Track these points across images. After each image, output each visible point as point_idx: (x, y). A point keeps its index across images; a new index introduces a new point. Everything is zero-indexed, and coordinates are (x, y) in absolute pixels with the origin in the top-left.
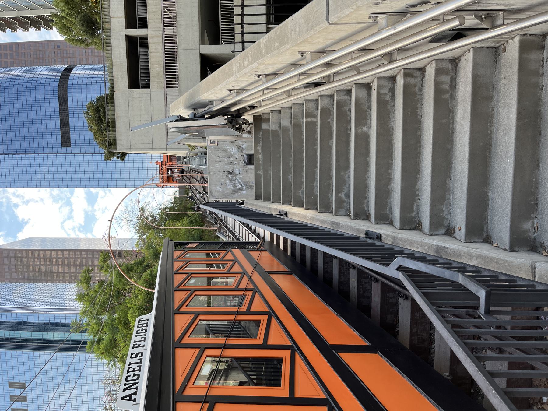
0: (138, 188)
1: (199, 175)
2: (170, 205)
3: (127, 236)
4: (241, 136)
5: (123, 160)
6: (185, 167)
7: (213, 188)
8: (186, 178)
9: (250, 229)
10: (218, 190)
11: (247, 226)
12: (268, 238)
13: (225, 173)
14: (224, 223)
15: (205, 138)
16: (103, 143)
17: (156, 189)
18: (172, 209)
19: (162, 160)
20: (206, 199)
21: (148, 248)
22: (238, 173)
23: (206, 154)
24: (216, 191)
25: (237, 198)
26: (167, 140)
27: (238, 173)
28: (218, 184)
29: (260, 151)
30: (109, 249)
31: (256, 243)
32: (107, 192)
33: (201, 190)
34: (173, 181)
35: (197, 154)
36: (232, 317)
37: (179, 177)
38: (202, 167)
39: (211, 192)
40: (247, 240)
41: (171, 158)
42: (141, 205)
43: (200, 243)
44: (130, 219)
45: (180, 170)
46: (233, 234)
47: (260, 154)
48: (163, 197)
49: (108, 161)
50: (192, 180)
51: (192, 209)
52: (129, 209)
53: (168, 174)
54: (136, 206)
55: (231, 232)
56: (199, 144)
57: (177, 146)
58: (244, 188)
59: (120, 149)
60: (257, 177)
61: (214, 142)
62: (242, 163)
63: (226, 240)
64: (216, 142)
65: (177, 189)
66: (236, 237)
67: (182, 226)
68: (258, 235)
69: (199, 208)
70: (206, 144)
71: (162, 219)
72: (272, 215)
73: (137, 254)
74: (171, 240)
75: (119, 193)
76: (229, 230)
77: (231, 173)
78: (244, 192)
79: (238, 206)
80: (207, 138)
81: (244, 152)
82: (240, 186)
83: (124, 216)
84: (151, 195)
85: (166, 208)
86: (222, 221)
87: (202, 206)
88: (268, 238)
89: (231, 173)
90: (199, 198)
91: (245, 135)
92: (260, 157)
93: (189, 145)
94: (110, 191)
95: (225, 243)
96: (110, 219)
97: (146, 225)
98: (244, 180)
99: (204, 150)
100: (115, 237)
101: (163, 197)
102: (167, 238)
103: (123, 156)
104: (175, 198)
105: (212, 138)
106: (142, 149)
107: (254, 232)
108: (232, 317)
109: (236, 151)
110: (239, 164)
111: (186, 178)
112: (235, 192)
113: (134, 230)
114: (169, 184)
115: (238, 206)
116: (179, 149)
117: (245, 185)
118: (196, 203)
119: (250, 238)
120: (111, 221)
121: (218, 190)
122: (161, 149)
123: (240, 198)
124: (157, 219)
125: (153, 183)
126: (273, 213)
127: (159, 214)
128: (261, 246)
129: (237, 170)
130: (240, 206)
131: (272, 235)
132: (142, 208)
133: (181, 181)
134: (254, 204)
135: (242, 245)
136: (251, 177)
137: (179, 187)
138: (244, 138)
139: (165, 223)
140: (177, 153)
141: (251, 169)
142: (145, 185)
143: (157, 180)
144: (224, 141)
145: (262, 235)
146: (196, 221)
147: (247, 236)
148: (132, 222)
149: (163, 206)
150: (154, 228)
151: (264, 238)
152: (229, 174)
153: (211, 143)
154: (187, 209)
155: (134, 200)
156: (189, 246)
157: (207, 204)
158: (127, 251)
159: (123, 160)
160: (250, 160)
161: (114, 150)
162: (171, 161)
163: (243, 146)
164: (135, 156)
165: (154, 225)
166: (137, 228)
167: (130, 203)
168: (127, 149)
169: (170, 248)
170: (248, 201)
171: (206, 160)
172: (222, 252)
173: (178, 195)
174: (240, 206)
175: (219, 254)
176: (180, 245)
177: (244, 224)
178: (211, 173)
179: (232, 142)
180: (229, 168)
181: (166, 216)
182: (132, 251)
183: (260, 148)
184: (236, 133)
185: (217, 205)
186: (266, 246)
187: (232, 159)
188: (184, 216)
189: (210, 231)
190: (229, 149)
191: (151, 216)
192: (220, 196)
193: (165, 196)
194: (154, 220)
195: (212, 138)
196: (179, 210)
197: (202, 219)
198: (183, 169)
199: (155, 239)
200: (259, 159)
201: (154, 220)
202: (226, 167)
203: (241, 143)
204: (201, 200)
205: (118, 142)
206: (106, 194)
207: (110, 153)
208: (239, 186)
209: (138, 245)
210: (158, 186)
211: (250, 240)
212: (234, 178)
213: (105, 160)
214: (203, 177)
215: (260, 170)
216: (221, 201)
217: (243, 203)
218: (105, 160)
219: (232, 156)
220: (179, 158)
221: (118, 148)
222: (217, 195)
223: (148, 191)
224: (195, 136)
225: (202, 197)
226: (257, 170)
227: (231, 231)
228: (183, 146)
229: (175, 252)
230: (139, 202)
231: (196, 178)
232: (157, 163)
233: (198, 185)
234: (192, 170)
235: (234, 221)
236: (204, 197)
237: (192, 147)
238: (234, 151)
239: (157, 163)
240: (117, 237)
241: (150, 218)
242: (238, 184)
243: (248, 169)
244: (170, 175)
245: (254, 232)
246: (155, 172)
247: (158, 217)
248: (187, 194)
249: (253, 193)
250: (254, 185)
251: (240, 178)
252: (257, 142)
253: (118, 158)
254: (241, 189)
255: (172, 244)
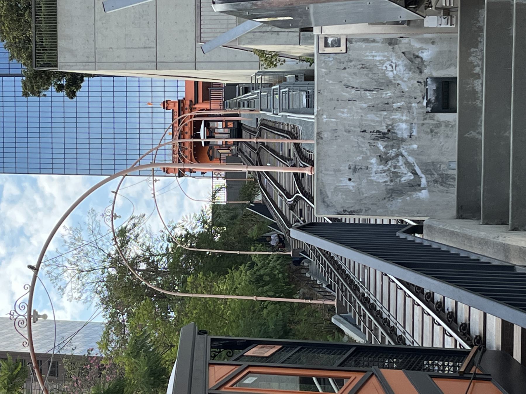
0: (112, 177)
1: (285, 141)
2: (199, 229)
3: (77, 313)
4: (419, 25)
5: (72, 95)
6: (246, 117)
7: (329, 180)
8: (247, 150)
9: (439, 309)
10: (345, 179)
11: (428, 299)
12: (494, 339)
13: (368, 135)
14: (356, 289)
15: (311, 30)
16: (21, 47)
17: (162, 180)
18: (204, 239)
19: (182, 95)
20: (306, 212)
21: (135, 353)
22: (406, 135)
23: (309, 77)
24: (337, 190)
25: (399, 214)
26: (199, 38)
27: (406, 135)
28: (344, 168)
29: (477, 70)
30: (27, 350)
31: (456, 355)
32: (26, 184)
33: (291, 185)
34: (211, 158)
35: (281, 79)
36: (227, 155)
37: (227, 146)
38: (296, 116)
39: (321, 192)
40: (427, 344)
41: (206, 90)
42: (118, 225)
43: (286, 346)
44: (86, 266)
45: (230, 125)
46: (385, 323)
47: (478, 76)
48: (180, 206)
49: (31, 98)
50: (266, 155)
51: (264, 241)
52: (85, 236)
53: (198, 136)
54: (106, 226)
55: (378, 315)
56: (291, 48)
57: (226, 54)
58: (424, 181)
59: (67, 63)
60: (466, 148)
61: (337, 43)
62: (420, 106)
63: (359, 340)
64: (343, 42)
65: (222, 182)
66: (392, 332)
67: (230, 294)
68: (464, 330)
69: (283, 242)
70: (311, 49)
71: (175, 268)
72: (512, 268)
73: (102, 368)
74: (202, 332)
75: (58, 189)
76: (372, 308)
77: (383, 136)
78: (424, 194)
79: (402, 236)
80: (316, 31)
81: (427, 71)
82: (410, 176)
83: (69, 256)
84: (148, 196)
85: (188, 236)
86: (351, 283)
87: (295, 234)
88: (494, 339)
89: (383, 136)
90: (285, 209)
91: (431, 21)
92: (478, 88)
93: (262, 53)
94: (34, 183)
95: (360, 350)
96: (34, 264)
97: (129, 285)
98: (425, 158)
99: (306, 65)
100: (45, 316)
101: (180, 206)
102: (189, 327)
103: (74, 82)
104: (215, 208)
105: (331, 31)
106: (126, 65)
107: (451, 319)
108: (227, 155)
109: (401, 68)
110: (409, 109)
111: (247, 150)
112: (395, 192)
113: (97, 299)
114: (198, 167)
115: (402, 236)
116: (230, 64)
117: (426, 172)
118: (275, 225)
119: (438, 336)
120: (36, 269)
121: (345, 179)
122: (180, 64)
123: (409, 213)
124: (161, 268)
125: (153, 164)
126: (514, 262)
127: (167, 254)
128: (471, 364)
129: (404, 126)
130: (410, 238)
131: (507, 329)
132: (123, 232)
133: (232, 159)
134: (452, 233)
135: (414, 358)
136: (446, 150)
137: (228, 175)
138: (430, 30)
139: (185, 281)
140: (224, 76)
141: (447, 124)
142: (133, 168)
143: (166, 154)
144: (366, 40)
145: (476, 329)
146: (274, 280)
147: (427, 332)
148: (92, 277)
149: (179, 232)
150: (152, 293)
151: (481, 341)
152: (377, 139)
153: (326, 45)
154: (247, 243)
155: (100, 211)
156: (253, 352)
157: (309, 227)
158: (74, 359)
159: (72, 95)
160: (444, 97)
161: (48, 65)
162: (207, 98)
163: (426, 55)
164: (107, 83)
165: (152, 285)
166: (106, 294)
167: (87, 219)
168: (86, 63)
169: (199, 354)
170: (435, 223)
171: (310, 98)
172: (352, 375)
173: (222, 198)
174: (410, 238)
175: (339, 382)
176: (228, 348)
177: (418, 291)
178: (325, 135)
179: (392, 42)
180: (377, 121)
181: (186, 260)
182: (87, 359)
183: (481, 67)
184: (405, 14)
185: (336, 231)
186: (490, 366)
187: (388, 94)
188: (237, 262)
189: (313, 311)
190: (382, 62)
191: (146, 260)
192: (350, 204)
193: (186, 202)
194: (153, 270)
195: (331, 31)
196: (225, 244)
197: (293, 271)
198: (239, 124)
199: (155, 327)
200: (473, 94)
201: (153, 270)
202: (371, 116)
203: (417, 45)
204: (290, 215)
205: (61, 43)
206: (22, 189)
207: (38, 74)
208: (408, 177)
209: (105, 344)
210: (166, 171)
211: (438, 345)
212: (392, 152)
213: (25, 94)
214: (297, 146)
215: (475, 126)
216: (350, 219)
217: (418, 228)
218: (25, 94)
219: (389, 83)
220: (231, 90)
221: (61, 59)
222: (339, 200)
223: (138, 188)
224: (284, 25)
225: (292, 207)
226: (466, 125)
227: (380, 313)
228: (242, 55)
229: (212, 369)
230: (114, 216)
231: (278, 149)
232: (166, 104)
233: (282, 171)
234: (266, 126)
235: (384, 280)
236: (298, 207)
237: (270, 59)
238: (395, 68)
239: (166, 104)
240: (50, 317)
241: (143, 266)
242: (404, 169)
243: (438, 125)
244: (203, 140)
245: (451, 319)
246: (159, 129)
247: (163, 264)
248: (250, 197)
249: (451, 196)
250: (455, 172)
251: (412, 153)
252: (468, 40)
253: (60, 88)
254: (415, 186)
255: (203, 344)
